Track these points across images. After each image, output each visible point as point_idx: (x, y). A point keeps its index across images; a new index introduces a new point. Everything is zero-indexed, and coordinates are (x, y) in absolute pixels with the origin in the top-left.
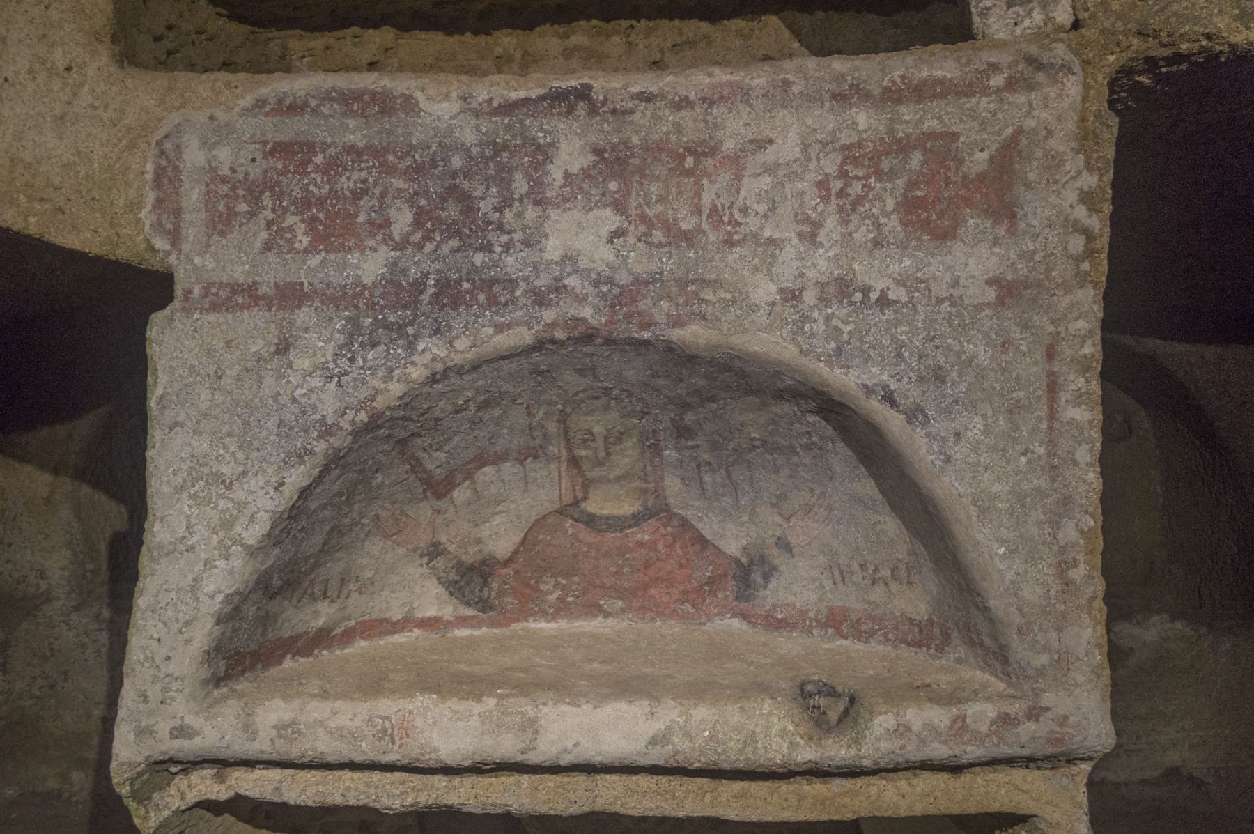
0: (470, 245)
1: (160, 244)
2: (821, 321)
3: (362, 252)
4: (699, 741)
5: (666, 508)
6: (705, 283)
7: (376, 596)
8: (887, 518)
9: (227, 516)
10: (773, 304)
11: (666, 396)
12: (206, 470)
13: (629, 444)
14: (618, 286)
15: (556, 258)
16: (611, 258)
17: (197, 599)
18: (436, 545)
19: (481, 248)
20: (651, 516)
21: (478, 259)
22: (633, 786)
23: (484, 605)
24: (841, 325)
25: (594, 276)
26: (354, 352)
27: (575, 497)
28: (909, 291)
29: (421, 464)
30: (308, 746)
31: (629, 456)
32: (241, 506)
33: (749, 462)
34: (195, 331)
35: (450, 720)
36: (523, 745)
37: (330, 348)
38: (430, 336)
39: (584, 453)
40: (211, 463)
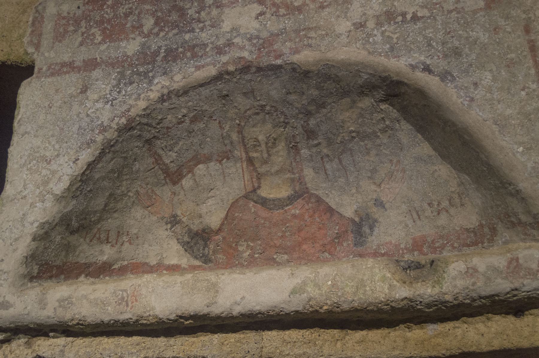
0: (183, 31)
1: (31, 50)
2: (379, 35)
3: (128, 40)
4: (325, 289)
5: (307, 191)
6: (309, 29)
7: (140, 247)
8: (440, 167)
9: (46, 178)
10: (350, 31)
11: (297, 108)
12: (38, 155)
13: (280, 147)
14: (262, 39)
15: (228, 30)
16: (258, 26)
17: (23, 226)
18: (175, 216)
19: (189, 31)
20: (299, 196)
21: (187, 37)
22: (286, 338)
23: (206, 260)
24: (391, 35)
25: (248, 36)
26: (121, 88)
27: (253, 186)
28: (429, 10)
29: (161, 159)
30: (76, 312)
31: (282, 156)
32: (54, 173)
33: (350, 150)
34: (41, 87)
35: (163, 287)
36: (208, 301)
37: (109, 88)
38: (161, 76)
39: (255, 155)
40: (41, 151)
